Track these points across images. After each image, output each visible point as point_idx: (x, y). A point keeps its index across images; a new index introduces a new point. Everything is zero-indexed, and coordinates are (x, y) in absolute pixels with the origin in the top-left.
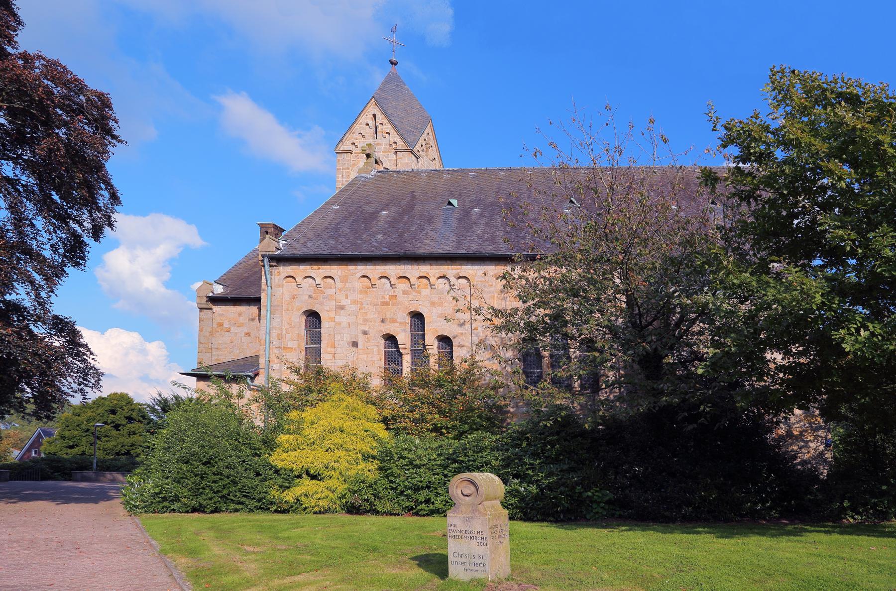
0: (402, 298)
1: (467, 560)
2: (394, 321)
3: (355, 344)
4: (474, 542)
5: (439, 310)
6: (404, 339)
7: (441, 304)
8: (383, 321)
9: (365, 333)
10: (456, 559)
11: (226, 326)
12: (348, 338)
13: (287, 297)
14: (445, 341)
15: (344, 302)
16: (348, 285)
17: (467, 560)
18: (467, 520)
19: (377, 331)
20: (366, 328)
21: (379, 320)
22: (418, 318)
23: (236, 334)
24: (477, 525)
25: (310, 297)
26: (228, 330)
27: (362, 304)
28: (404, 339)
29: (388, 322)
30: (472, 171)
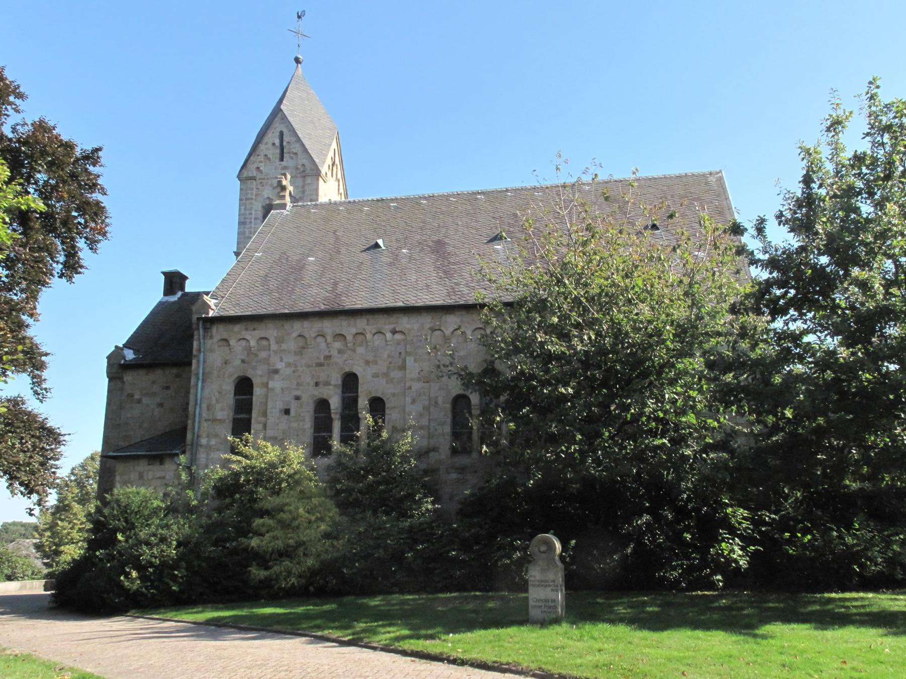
0: (337, 359)
1: (543, 604)
2: (327, 384)
3: (287, 412)
4: (549, 589)
5: (373, 369)
6: (335, 403)
7: (375, 363)
8: (317, 384)
9: (297, 398)
10: (534, 604)
11: (137, 397)
12: (280, 405)
13: (219, 362)
14: (377, 405)
15: (280, 366)
16: (284, 346)
17: (543, 604)
18: (543, 571)
19: (310, 395)
20: (298, 393)
21: (312, 383)
22: (350, 381)
23: (148, 405)
24: (551, 576)
25: (243, 361)
26: (139, 401)
27: (296, 366)
28: (335, 403)
29: (321, 385)
30: (392, 200)
